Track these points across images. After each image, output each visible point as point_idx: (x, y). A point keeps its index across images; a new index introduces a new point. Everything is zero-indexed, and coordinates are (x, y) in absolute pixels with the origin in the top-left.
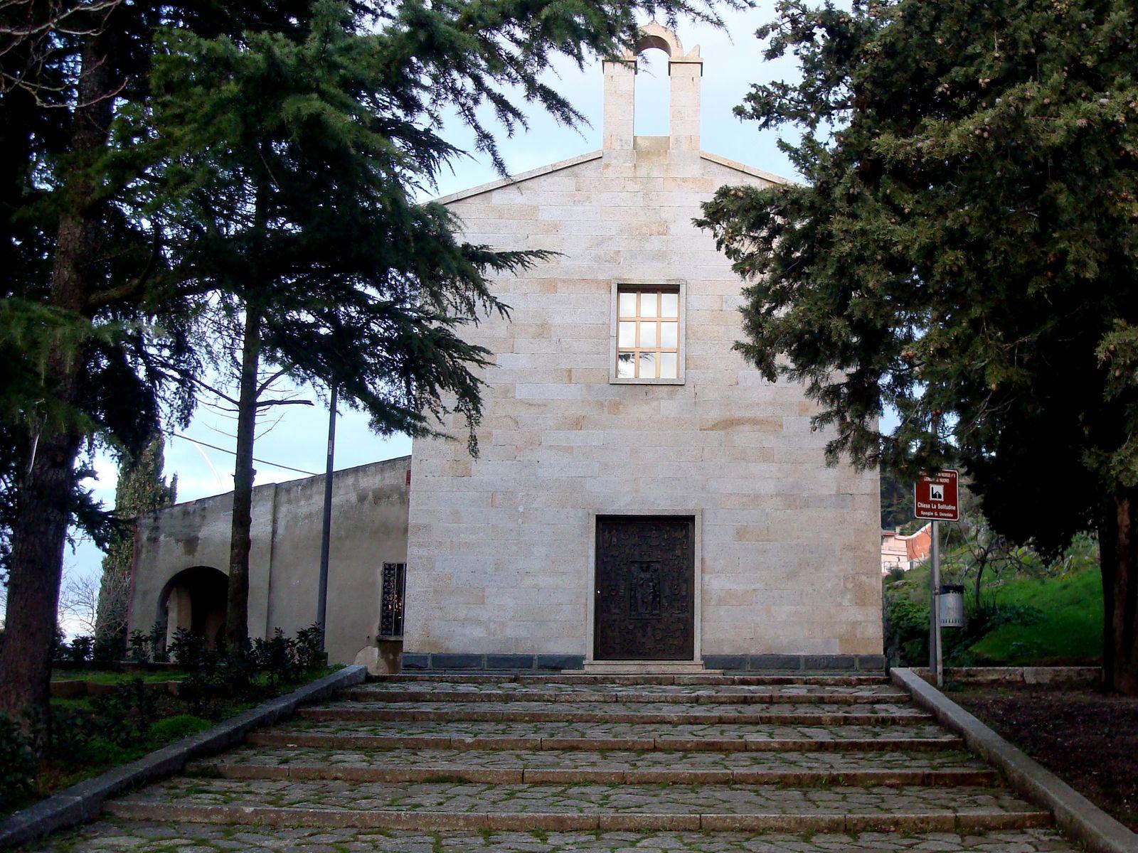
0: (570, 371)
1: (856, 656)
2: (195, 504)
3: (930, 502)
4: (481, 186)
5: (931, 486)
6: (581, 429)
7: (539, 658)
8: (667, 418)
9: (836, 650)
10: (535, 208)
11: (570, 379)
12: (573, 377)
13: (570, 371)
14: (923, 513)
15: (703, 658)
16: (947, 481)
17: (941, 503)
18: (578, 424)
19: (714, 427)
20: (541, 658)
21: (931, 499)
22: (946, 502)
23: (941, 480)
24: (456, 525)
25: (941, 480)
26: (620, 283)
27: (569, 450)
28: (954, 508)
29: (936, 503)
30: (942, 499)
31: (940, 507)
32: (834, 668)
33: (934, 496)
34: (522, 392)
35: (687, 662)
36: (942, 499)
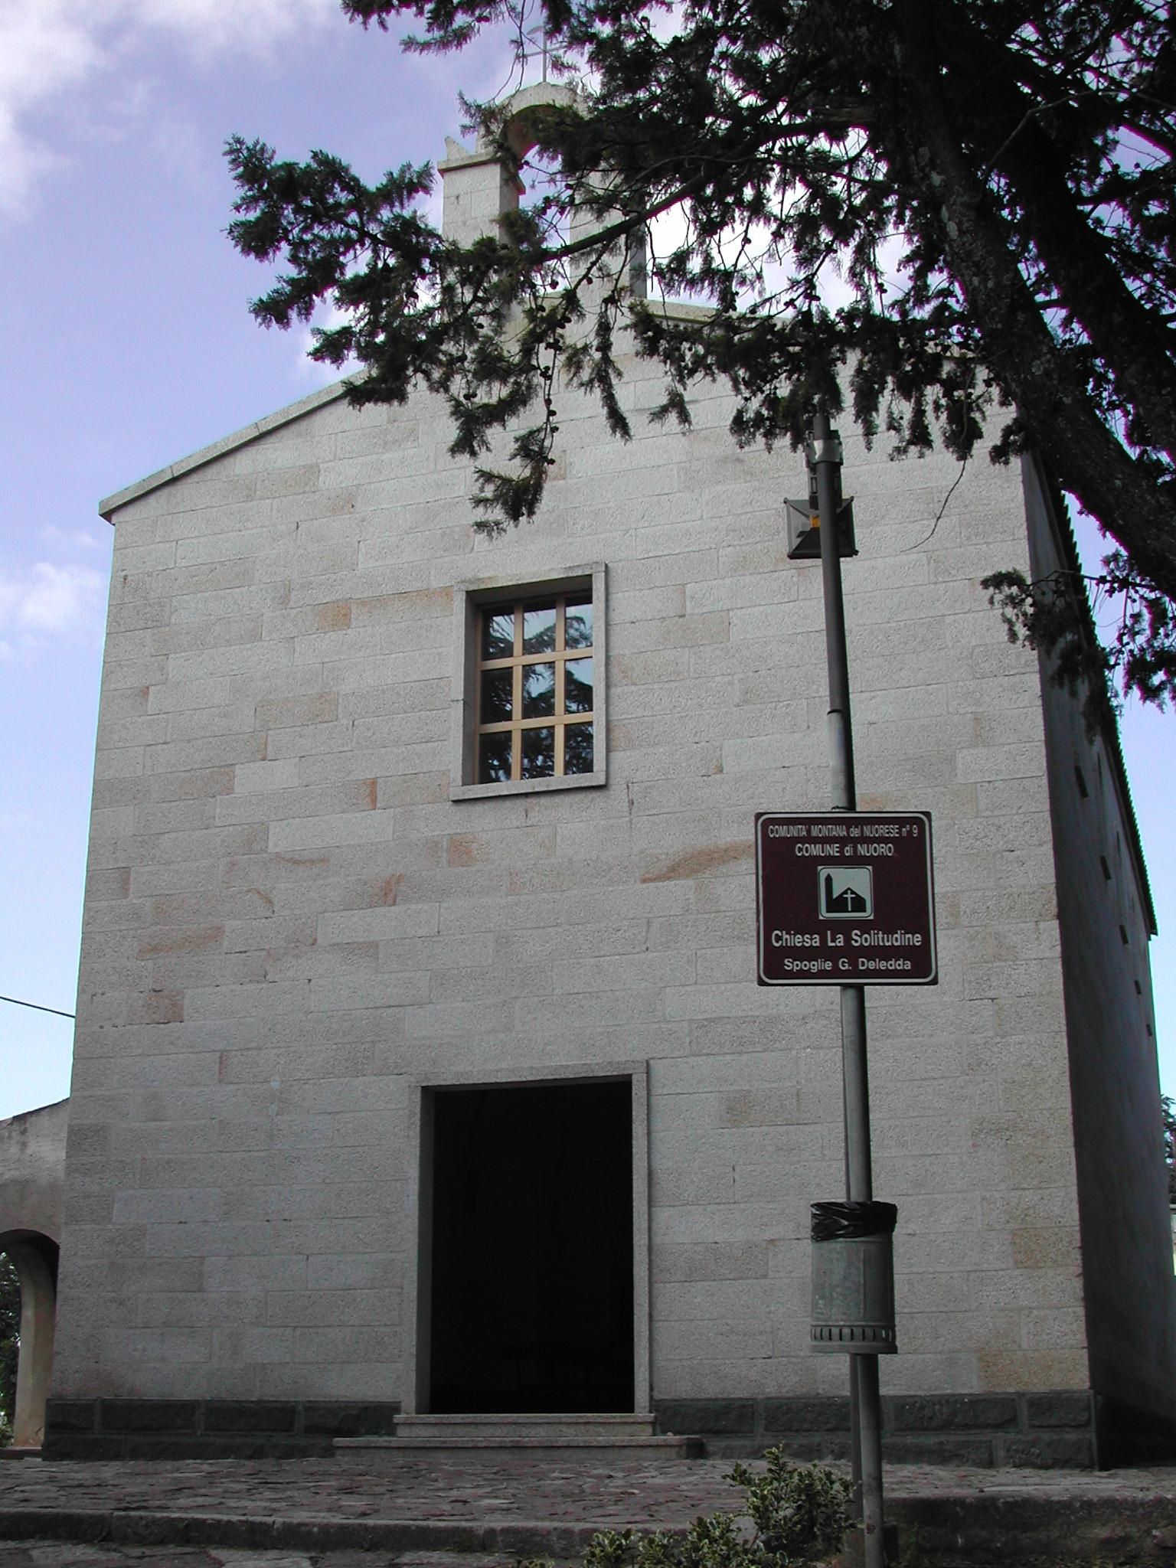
0: (373, 783)
1: (1021, 1395)
2: (11, 1124)
3: (820, 928)
4: (215, 446)
5: (823, 872)
6: (394, 903)
7: (307, 1409)
8: (570, 861)
9: (971, 1384)
10: (313, 470)
11: (374, 801)
12: (380, 795)
13: (373, 783)
14: (790, 965)
15: (654, 1405)
16: (885, 850)
17: (865, 927)
18: (389, 893)
19: (675, 871)
20: (311, 1407)
21: (824, 914)
22: (885, 921)
23: (862, 850)
24: (151, 1124)
25: (862, 850)
26: (472, 588)
27: (369, 950)
28: (917, 940)
29: (845, 927)
30: (868, 914)
31: (858, 939)
32: (967, 1426)
33: (837, 904)
34: (282, 839)
35: (617, 1417)
36: (868, 914)
